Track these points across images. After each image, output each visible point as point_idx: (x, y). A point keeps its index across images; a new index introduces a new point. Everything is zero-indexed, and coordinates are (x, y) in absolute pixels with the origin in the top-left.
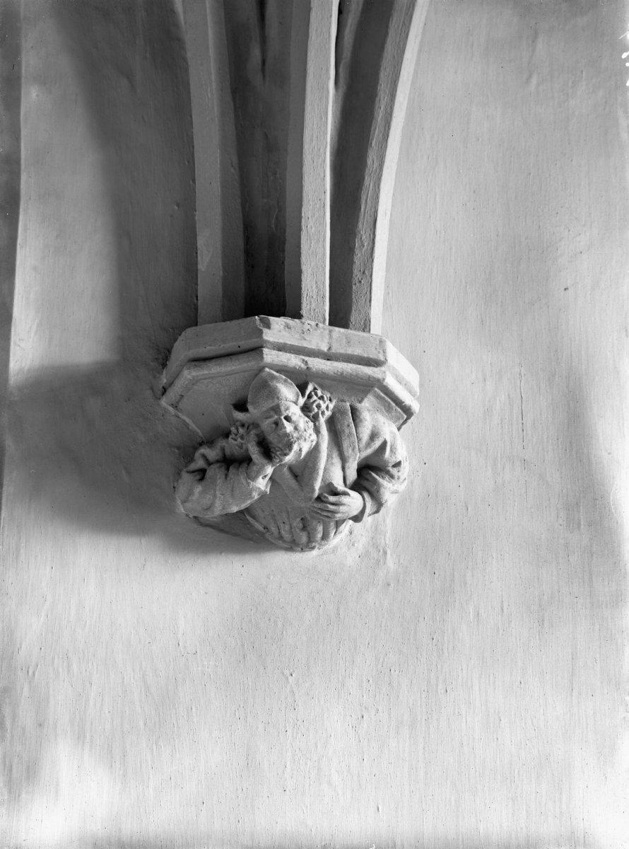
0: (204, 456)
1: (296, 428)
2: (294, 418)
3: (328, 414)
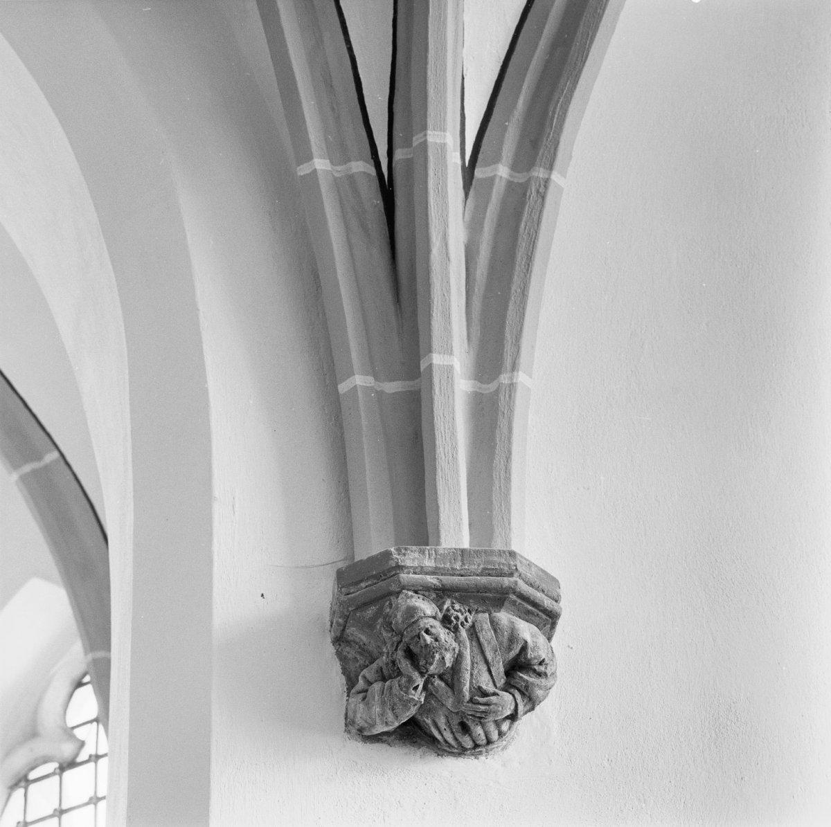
0: (364, 677)
1: (436, 640)
2: (433, 630)
3: (468, 625)
